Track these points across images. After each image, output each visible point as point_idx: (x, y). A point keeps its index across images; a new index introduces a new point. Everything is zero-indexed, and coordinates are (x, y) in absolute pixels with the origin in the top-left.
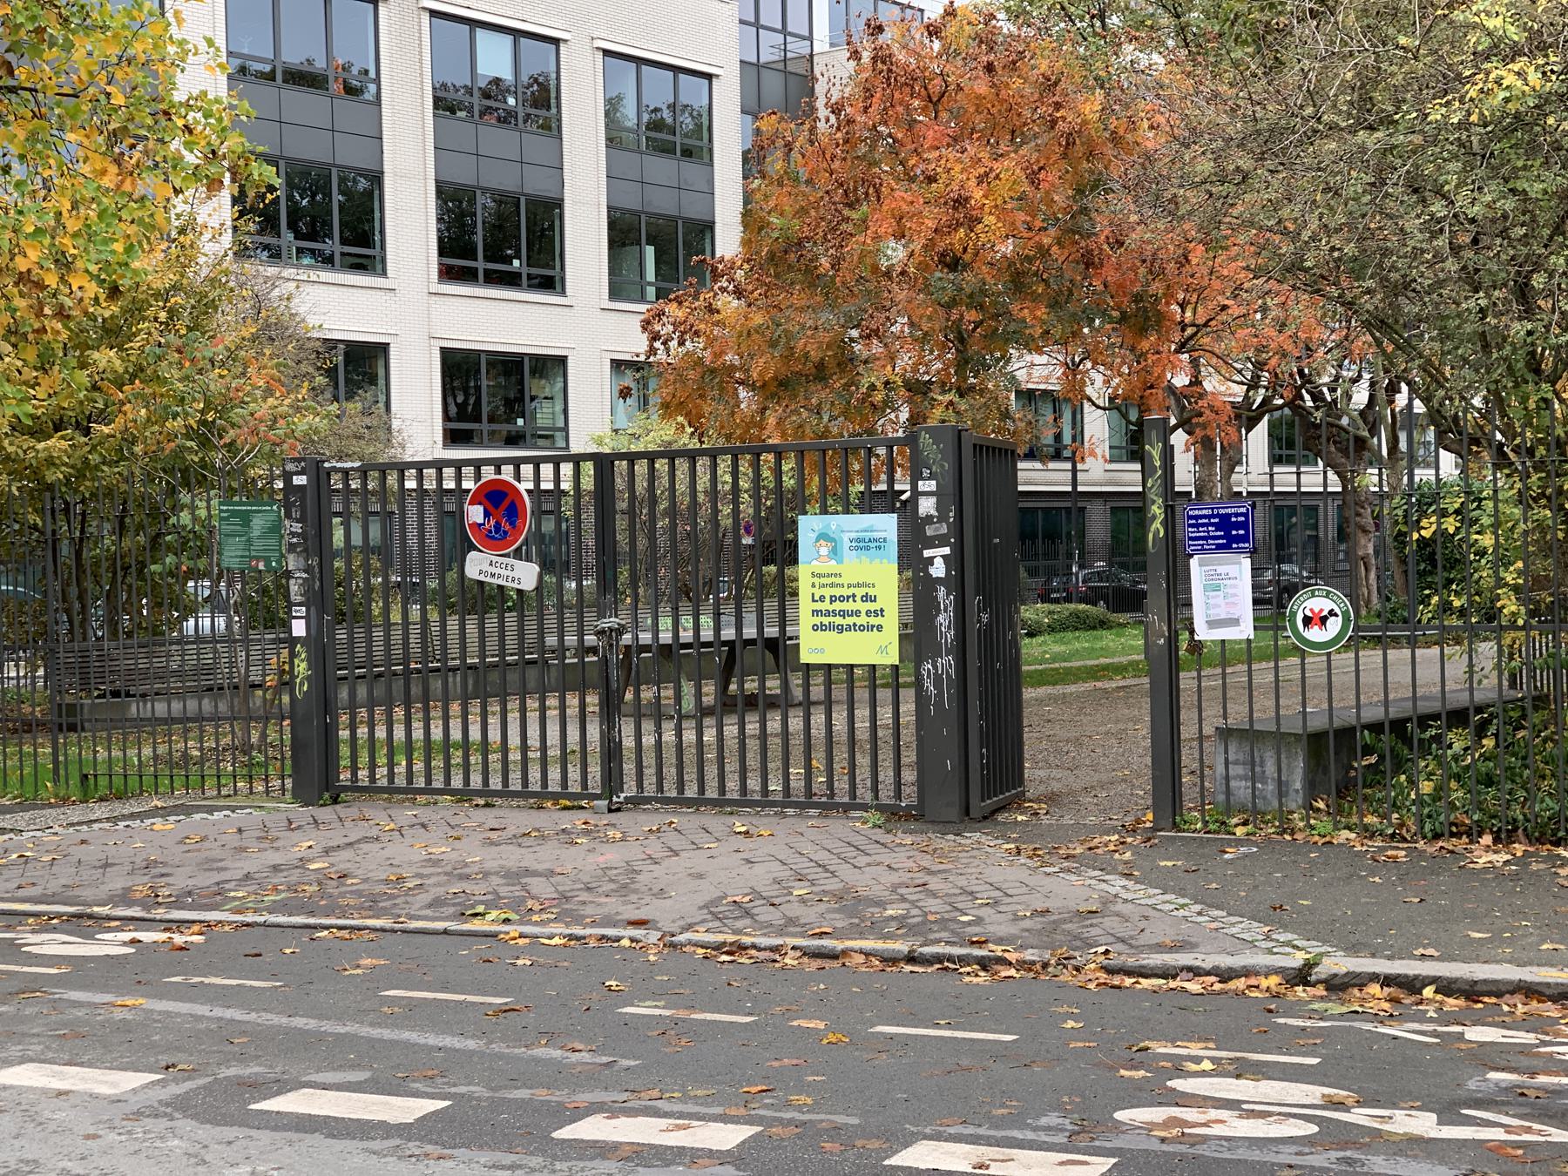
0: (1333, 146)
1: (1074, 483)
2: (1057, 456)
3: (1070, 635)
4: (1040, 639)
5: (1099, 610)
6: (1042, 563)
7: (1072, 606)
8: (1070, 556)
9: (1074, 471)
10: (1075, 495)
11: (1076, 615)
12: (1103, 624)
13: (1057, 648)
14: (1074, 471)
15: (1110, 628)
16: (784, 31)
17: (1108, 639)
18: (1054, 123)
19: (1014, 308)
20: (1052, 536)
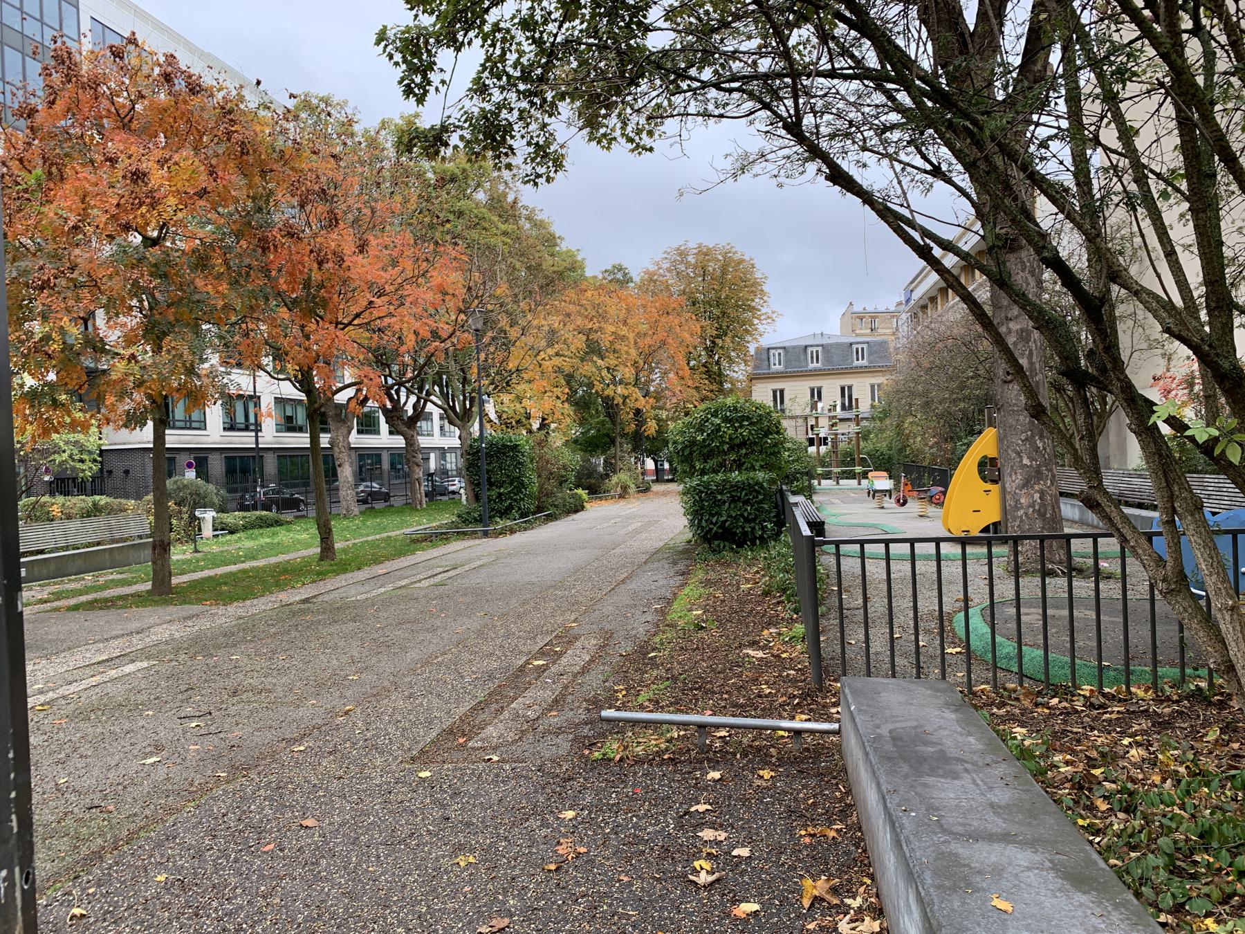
0: (286, 316)
1: (257, 443)
2: (247, 429)
3: (256, 531)
4: (235, 537)
5: (272, 514)
6: (238, 486)
7: (258, 513)
8: (256, 481)
9: (257, 437)
10: (257, 449)
11: (260, 518)
12: (278, 523)
13: (249, 544)
14: (257, 437)
15: (281, 525)
16: (41, 21)
17: (283, 535)
18: (229, 135)
19: (199, 283)
20: (245, 471)
